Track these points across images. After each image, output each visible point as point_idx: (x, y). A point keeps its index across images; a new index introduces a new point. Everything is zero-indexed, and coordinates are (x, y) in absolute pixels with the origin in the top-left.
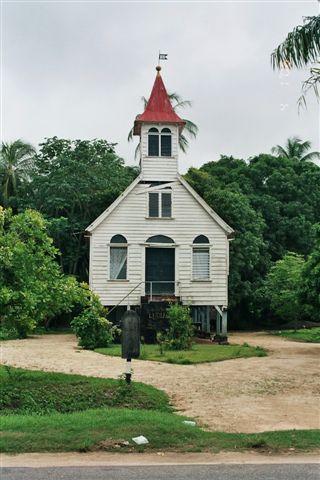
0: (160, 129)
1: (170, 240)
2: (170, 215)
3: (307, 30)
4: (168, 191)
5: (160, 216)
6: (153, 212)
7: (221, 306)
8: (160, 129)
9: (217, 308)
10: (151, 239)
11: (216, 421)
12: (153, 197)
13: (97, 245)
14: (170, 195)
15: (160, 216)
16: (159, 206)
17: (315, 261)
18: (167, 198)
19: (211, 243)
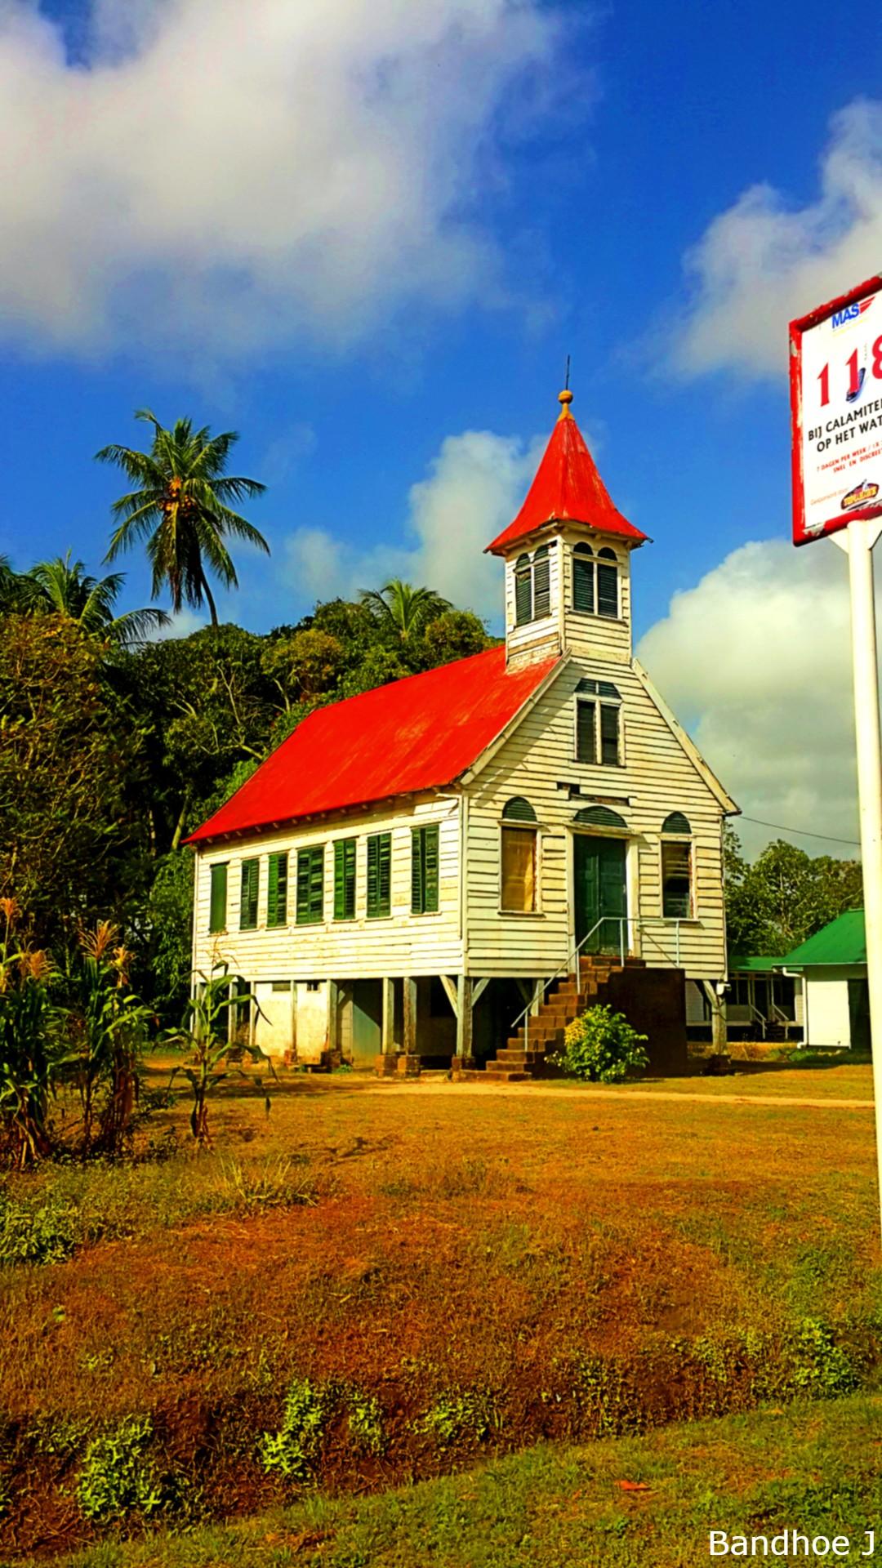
0: (596, 548)
1: (619, 821)
7: (714, 983)
8: (596, 548)
12: (585, 708)
18: (610, 713)
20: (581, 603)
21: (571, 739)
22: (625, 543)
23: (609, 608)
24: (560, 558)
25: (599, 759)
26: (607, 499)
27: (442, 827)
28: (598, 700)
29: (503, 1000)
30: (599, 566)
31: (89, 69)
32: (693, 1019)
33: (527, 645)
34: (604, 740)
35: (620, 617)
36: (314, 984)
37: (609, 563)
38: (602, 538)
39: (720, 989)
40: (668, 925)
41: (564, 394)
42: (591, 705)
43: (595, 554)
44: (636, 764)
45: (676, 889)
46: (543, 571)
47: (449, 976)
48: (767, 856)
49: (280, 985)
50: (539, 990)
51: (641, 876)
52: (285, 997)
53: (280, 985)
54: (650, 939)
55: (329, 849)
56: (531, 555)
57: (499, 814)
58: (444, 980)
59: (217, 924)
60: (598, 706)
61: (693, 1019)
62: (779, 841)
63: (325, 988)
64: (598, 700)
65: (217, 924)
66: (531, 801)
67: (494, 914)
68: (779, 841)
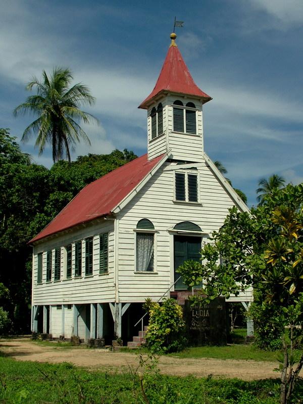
0: (185, 102)
1: (197, 227)
2: (196, 200)
3: (241, 309)
4: (193, 172)
5: (187, 200)
6: (180, 195)
7: (247, 303)
8: (185, 102)
9: (244, 305)
10: (178, 226)
11: (253, 363)
12: (180, 178)
13: (123, 231)
14: (196, 177)
15: (187, 200)
16: (186, 189)
17: (32, 167)
18: (193, 179)
19: (156, 228)
20: (178, 127)
21: (172, 194)
22: (199, 100)
23: (192, 129)
24: (168, 112)
26: (192, 80)
28: (186, 173)
29: (137, 313)
30: (187, 111)
31: (273, 176)
33: (154, 150)
35: (197, 134)
36: (69, 306)
38: (188, 98)
41: (173, 34)
43: (185, 105)
49: (59, 307)
52: (60, 311)
53: (59, 307)
57: (135, 227)
59: (40, 281)
62: (126, 150)
63: (73, 308)
65: (40, 281)
67: (132, 273)
68: (126, 150)
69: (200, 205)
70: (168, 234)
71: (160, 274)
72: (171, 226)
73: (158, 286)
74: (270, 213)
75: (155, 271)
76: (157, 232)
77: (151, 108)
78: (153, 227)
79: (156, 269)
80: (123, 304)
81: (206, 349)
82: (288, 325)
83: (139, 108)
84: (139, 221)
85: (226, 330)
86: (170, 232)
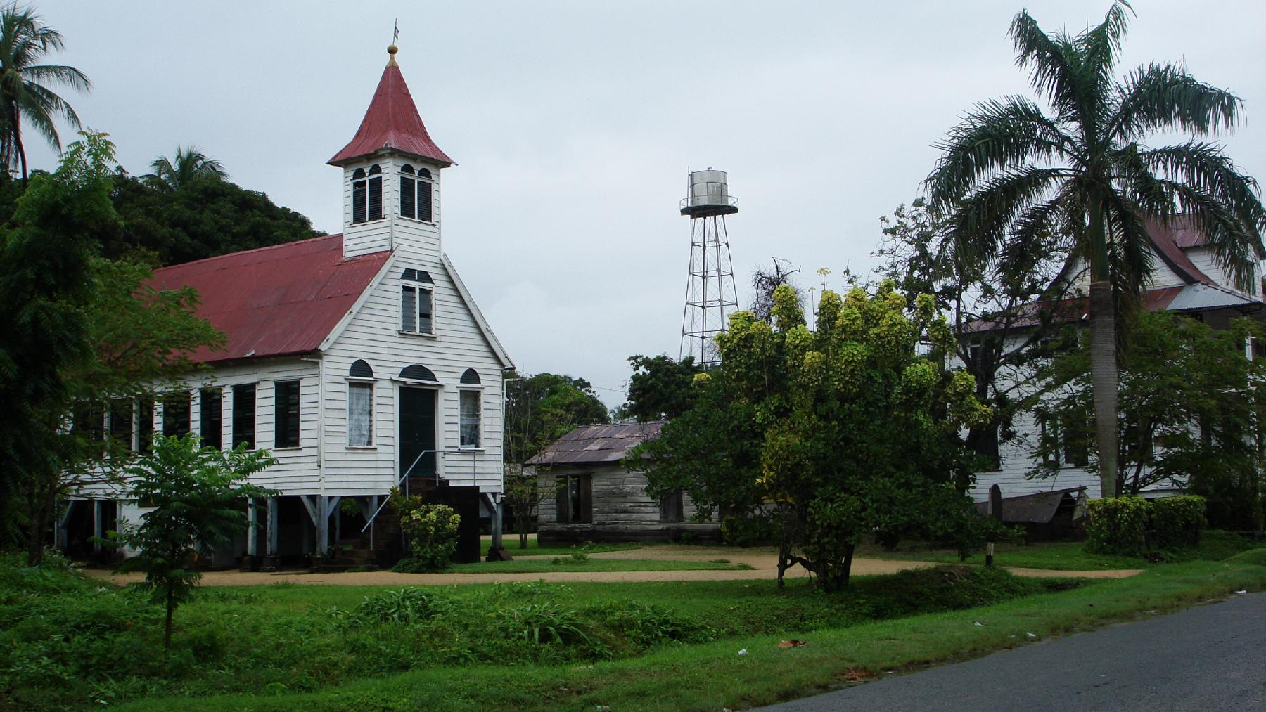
0: (417, 168)
4: (427, 286)
7: (494, 494)
8: (417, 168)
10: (406, 372)
18: (426, 293)
20: (407, 211)
25: (418, 330)
27: (302, 383)
32: (483, 513)
34: (421, 315)
37: (424, 180)
39: (498, 498)
40: (464, 453)
42: (412, 290)
44: (462, 470)
45: (471, 436)
46: (376, 186)
47: (309, 497)
48: (492, 690)
50: (375, 501)
51: (448, 418)
54: (453, 468)
55: (196, 394)
56: (367, 170)
58: (305, 501)
60: (417, 291)
61: (483, 513)
64: (418, 285)
66: (369, 362)
69: (434, 338)
70: (389, 384)
71: (380, 449)
72: (395, 373)
73: (377, 472)
74: (757, 662)
75: (374, 446)
76: (376, 380)
77: (355, 168)
78: (370, 373)
79: (376, 442)
80: (331, 498)
81: (561, 547)
82: (1187, 345)
83: (332, 163)
84: (353, 365)
85: (1214, 442)
86: (392, 381)
